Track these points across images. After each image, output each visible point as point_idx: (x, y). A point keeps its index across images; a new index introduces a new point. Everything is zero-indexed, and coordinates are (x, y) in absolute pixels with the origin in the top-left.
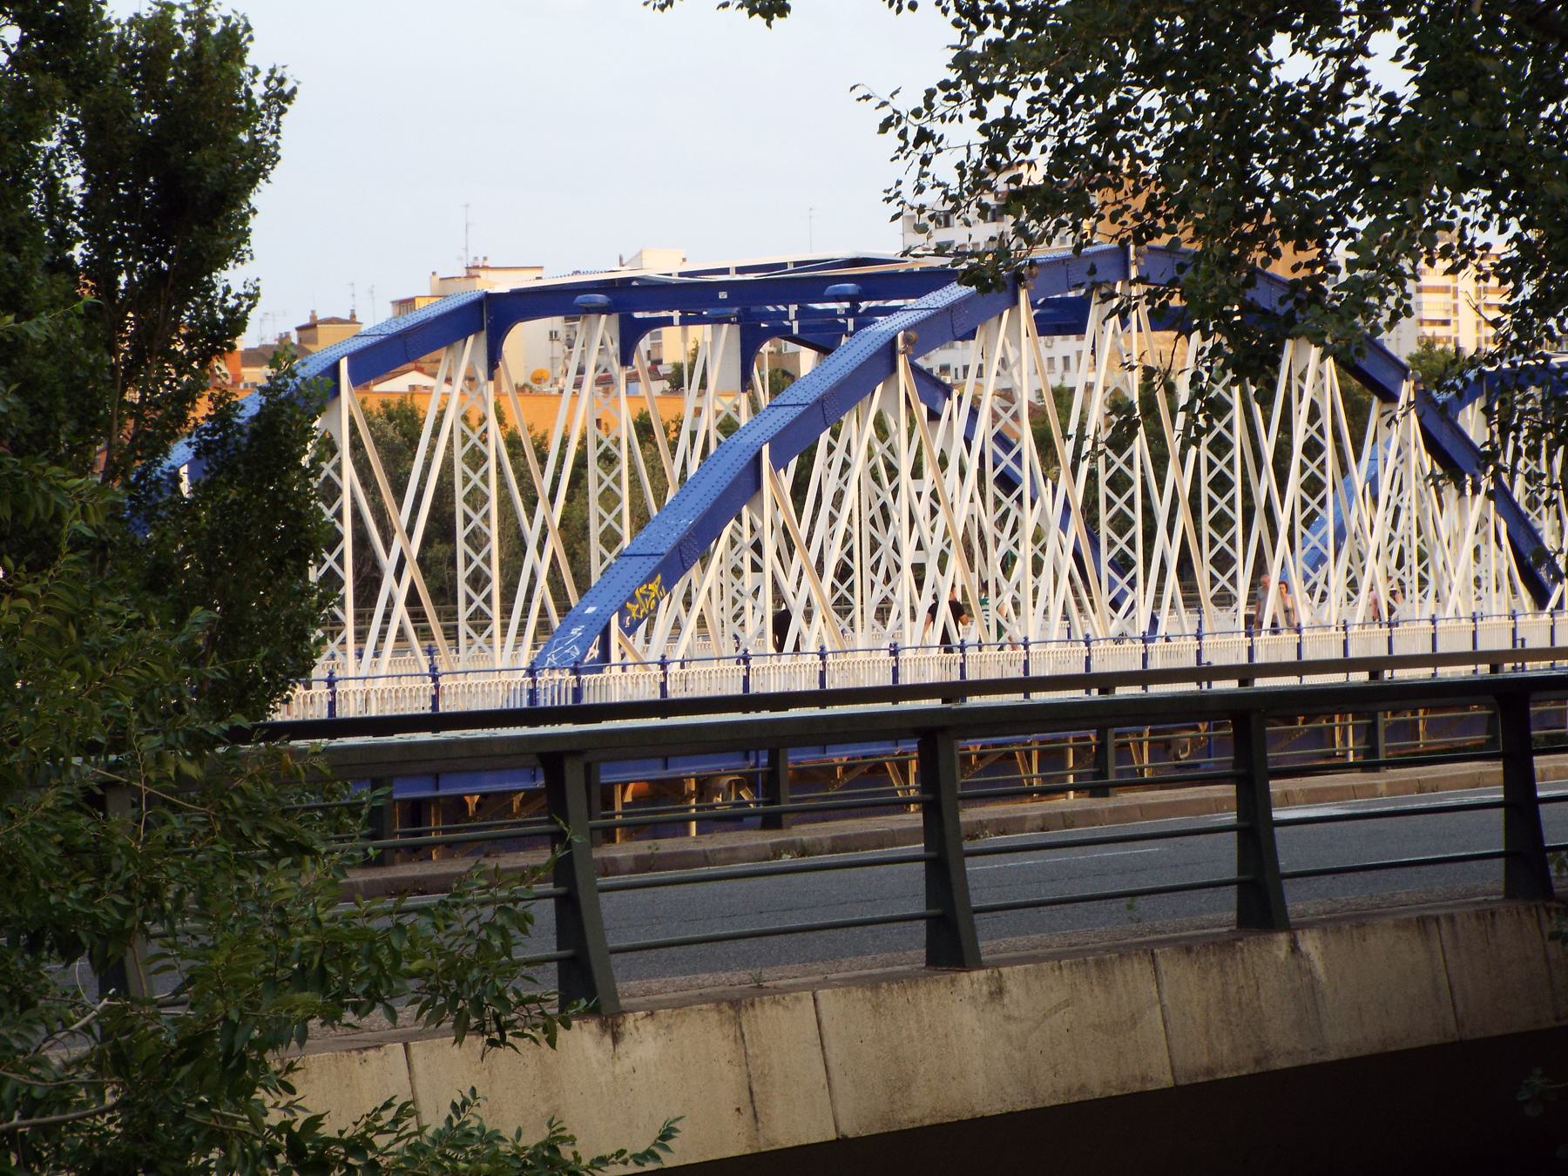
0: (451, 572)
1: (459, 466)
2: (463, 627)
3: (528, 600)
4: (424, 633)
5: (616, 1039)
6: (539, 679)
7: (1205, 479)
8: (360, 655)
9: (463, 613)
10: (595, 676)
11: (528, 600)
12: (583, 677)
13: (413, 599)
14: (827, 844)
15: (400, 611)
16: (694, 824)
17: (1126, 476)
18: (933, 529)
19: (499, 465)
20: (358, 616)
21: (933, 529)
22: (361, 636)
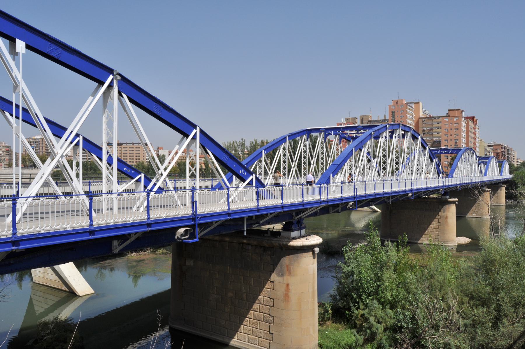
0: (222, 178)
1: (302, 153)
2: (302, 175)
3: (292, 174)
4: (297, 176)
5: (453, 240)
6: (283, 187)
7: (382, 161)
8: (288, 178)
9: (302, 173)
10: (263, 189)
11: (292, 174)
12: (259, 189)
13: (296, 171)
14: (305, 219)
15: (294, 173)
16: (331, 208)
17: (268, 172)
18: (361, 165)
19: (288, 157)
20: (288, 174)
21: (361, 165)
22: (288, 176)
